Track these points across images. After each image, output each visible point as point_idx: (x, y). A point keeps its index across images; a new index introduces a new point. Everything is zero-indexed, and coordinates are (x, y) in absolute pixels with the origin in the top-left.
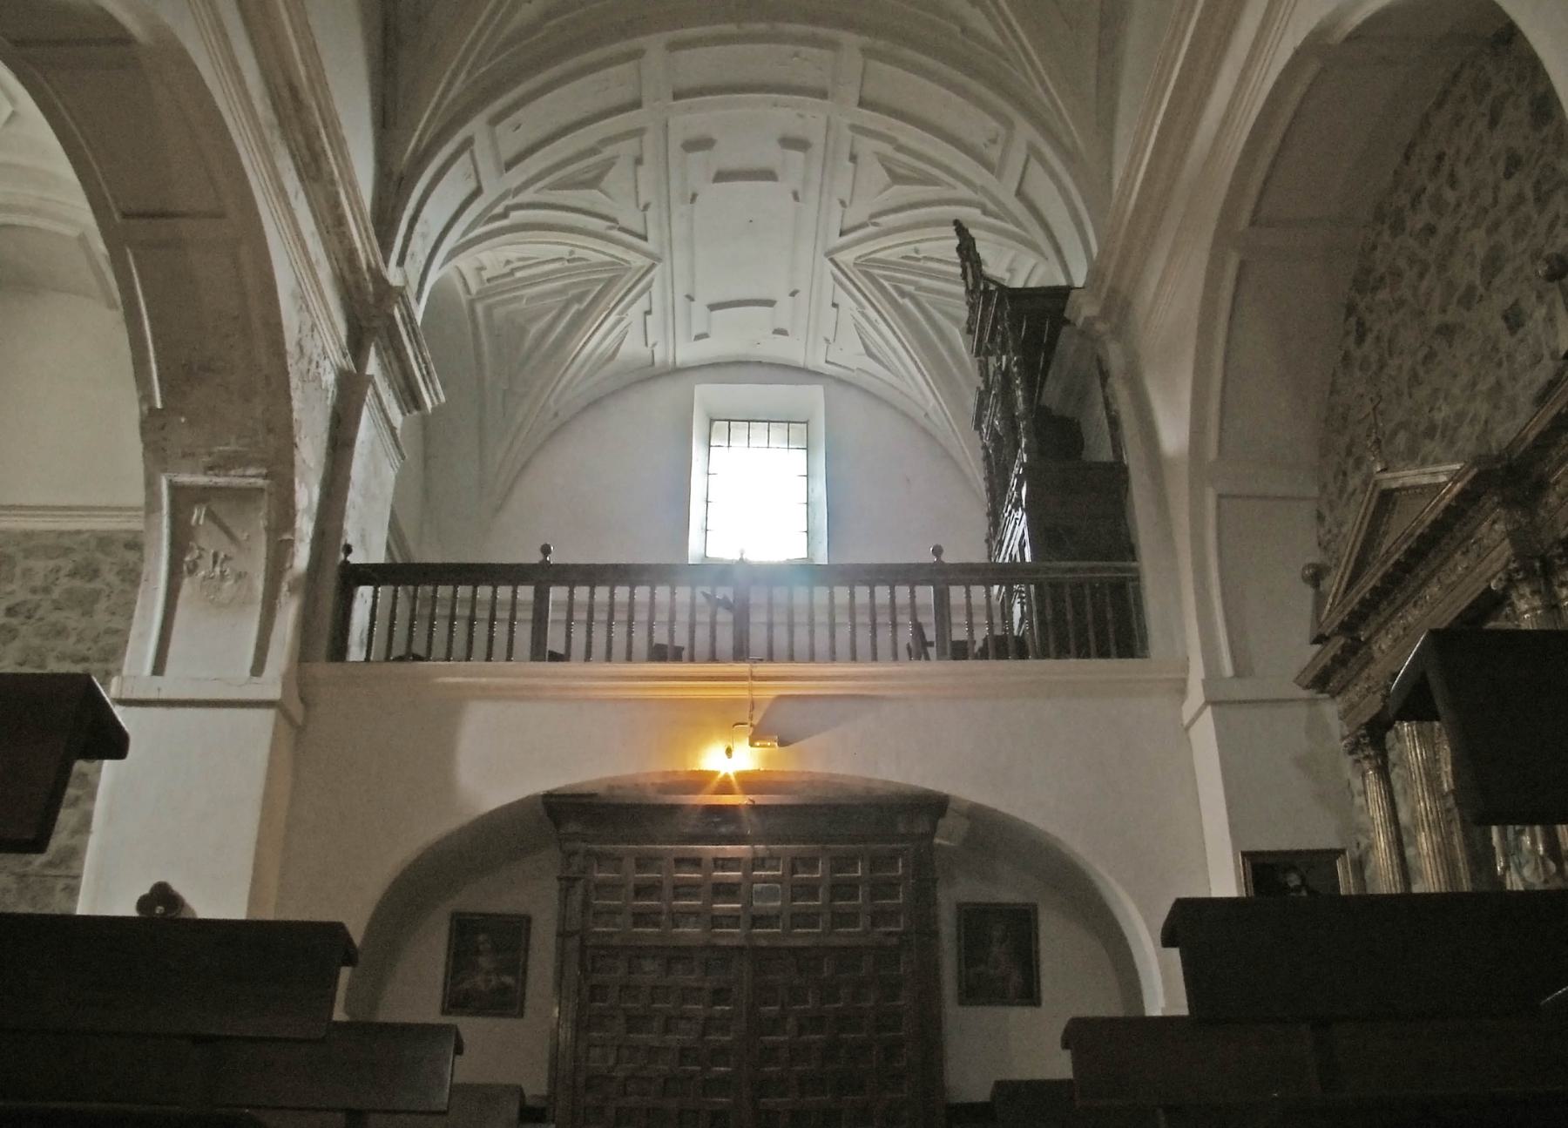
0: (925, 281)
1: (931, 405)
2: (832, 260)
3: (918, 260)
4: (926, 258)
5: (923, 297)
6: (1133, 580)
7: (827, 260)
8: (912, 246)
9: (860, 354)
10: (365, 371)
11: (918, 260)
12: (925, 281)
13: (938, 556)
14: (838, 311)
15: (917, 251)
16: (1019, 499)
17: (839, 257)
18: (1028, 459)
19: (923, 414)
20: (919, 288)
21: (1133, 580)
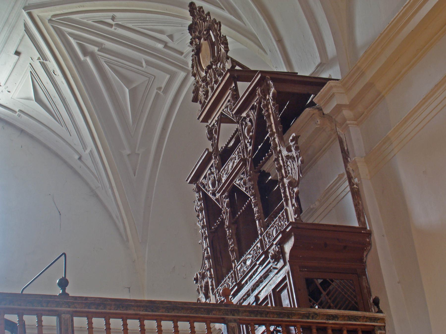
0: (109, 44)
1: (214, 160)
2: (30, 15)
3: (111, 25)
4: (118, 25)
5: (102, 57)
6: (380, 328)
7: (24, 13)
8: (111, 14)
9: (29, 99)
10: (215, 303)
11: (111, 25)
12: (109, 44)
13: (64, 290)
14: (18, 59)
15: (113, 18)
16: (282, 252)
17: (35, 12)
18: (242, 208)
19: (77, 157)
20: (102, 49)
21: (380, 328)
